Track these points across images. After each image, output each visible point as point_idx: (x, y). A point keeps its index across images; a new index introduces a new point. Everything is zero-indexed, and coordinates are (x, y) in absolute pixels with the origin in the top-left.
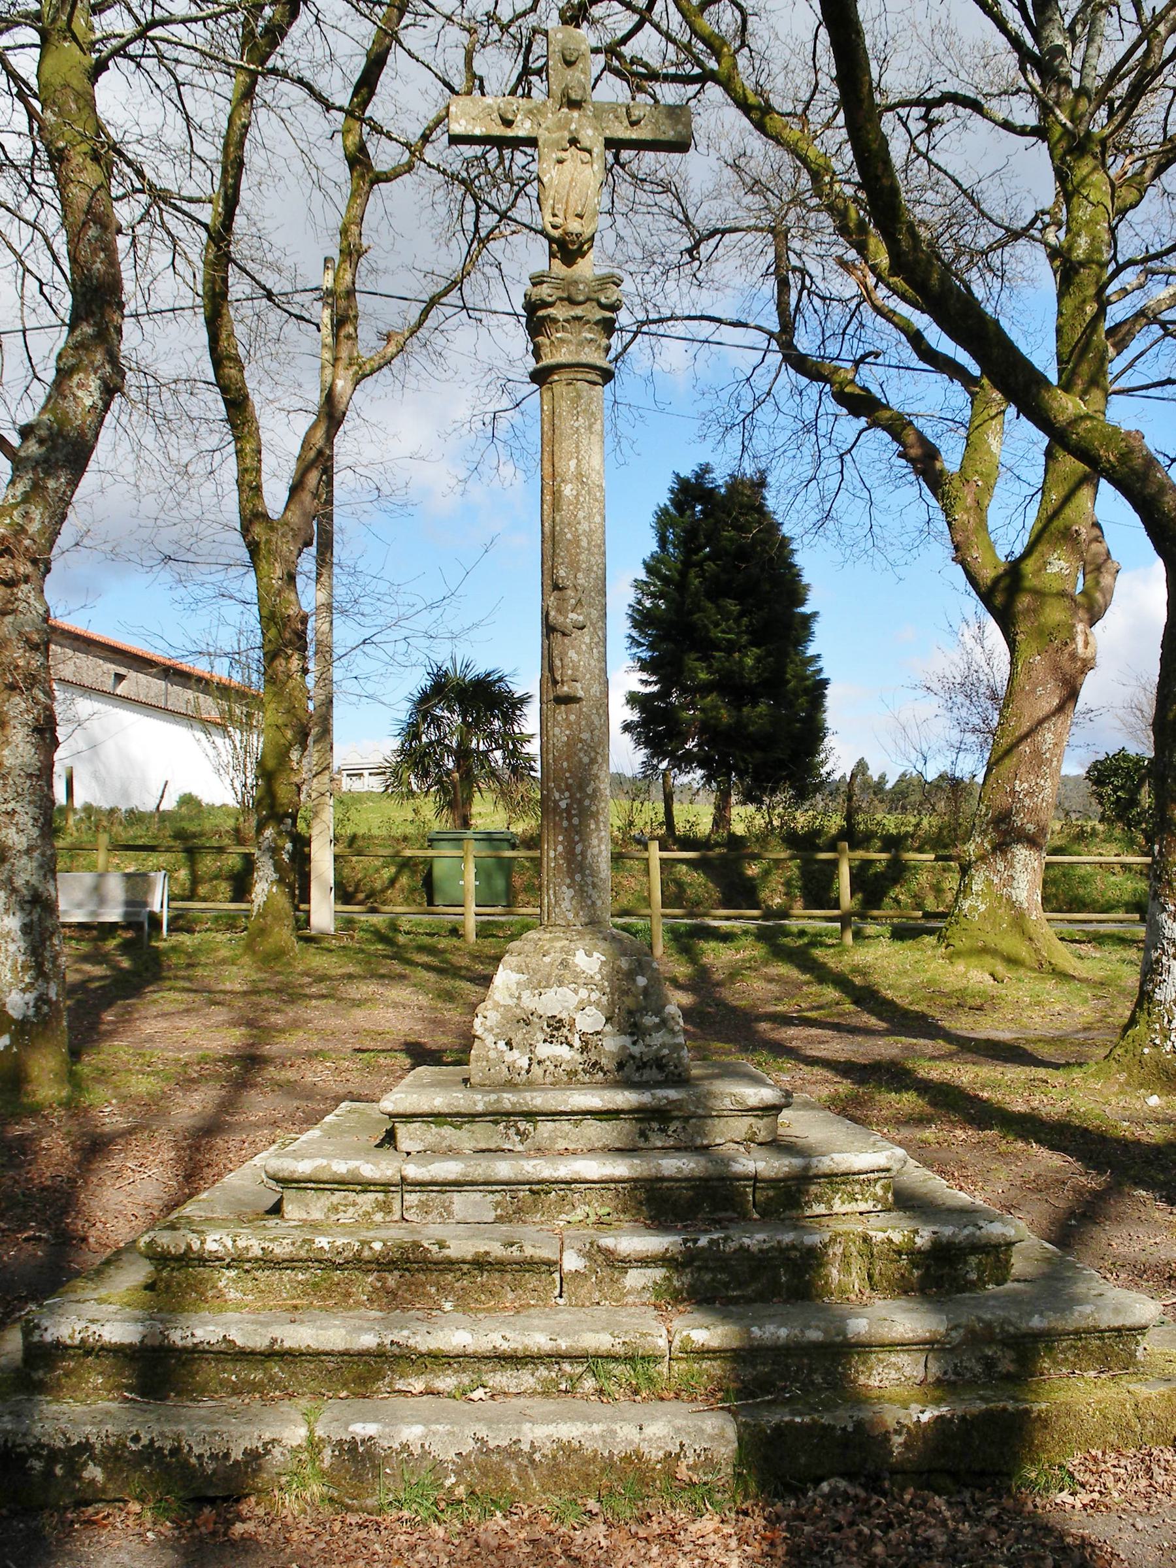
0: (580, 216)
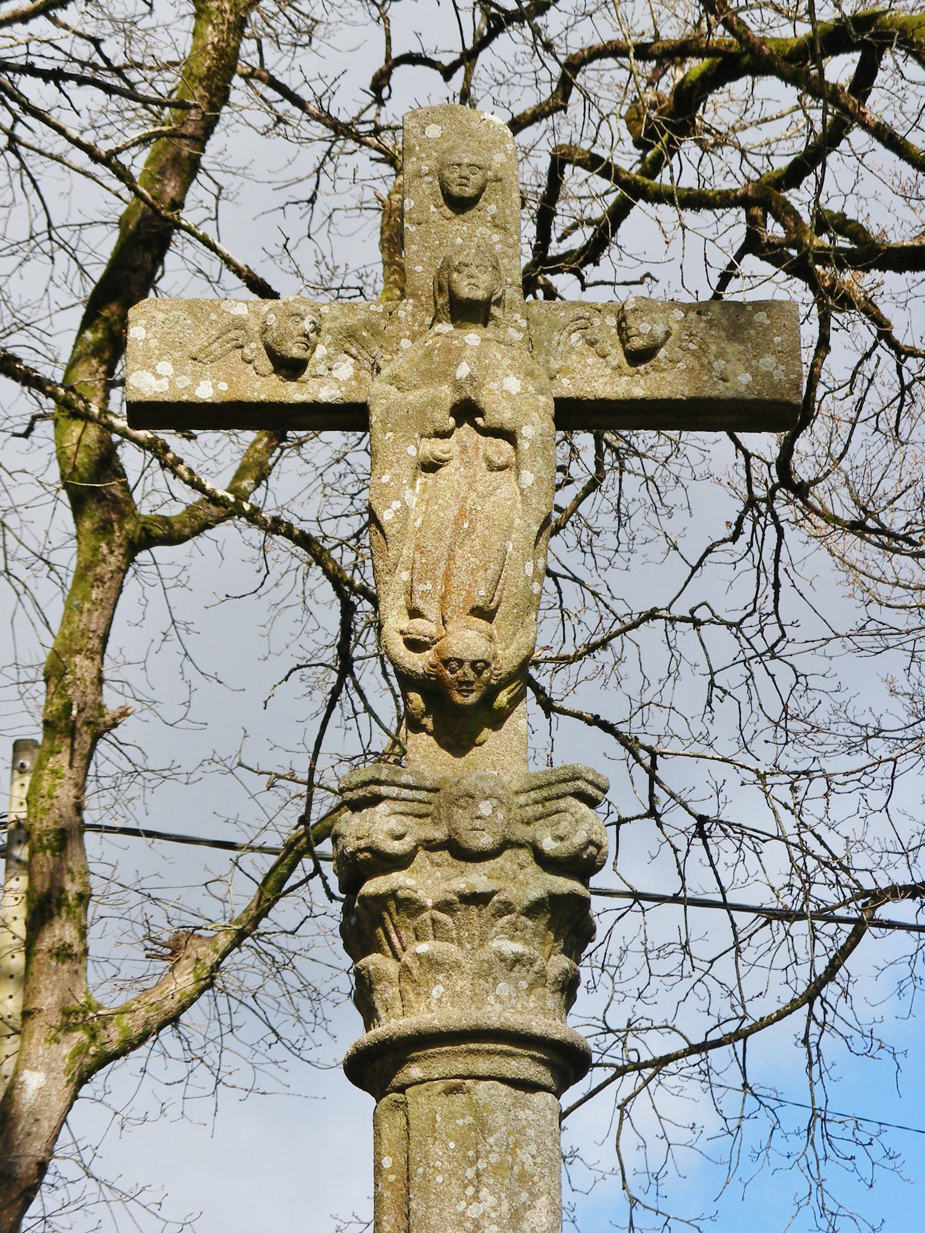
0: (485, 613)
